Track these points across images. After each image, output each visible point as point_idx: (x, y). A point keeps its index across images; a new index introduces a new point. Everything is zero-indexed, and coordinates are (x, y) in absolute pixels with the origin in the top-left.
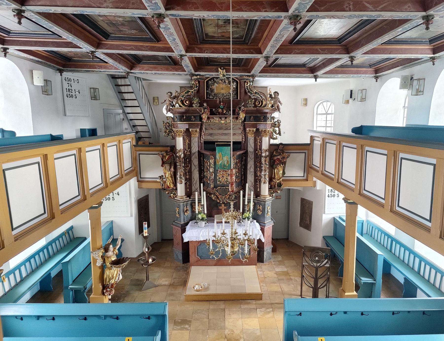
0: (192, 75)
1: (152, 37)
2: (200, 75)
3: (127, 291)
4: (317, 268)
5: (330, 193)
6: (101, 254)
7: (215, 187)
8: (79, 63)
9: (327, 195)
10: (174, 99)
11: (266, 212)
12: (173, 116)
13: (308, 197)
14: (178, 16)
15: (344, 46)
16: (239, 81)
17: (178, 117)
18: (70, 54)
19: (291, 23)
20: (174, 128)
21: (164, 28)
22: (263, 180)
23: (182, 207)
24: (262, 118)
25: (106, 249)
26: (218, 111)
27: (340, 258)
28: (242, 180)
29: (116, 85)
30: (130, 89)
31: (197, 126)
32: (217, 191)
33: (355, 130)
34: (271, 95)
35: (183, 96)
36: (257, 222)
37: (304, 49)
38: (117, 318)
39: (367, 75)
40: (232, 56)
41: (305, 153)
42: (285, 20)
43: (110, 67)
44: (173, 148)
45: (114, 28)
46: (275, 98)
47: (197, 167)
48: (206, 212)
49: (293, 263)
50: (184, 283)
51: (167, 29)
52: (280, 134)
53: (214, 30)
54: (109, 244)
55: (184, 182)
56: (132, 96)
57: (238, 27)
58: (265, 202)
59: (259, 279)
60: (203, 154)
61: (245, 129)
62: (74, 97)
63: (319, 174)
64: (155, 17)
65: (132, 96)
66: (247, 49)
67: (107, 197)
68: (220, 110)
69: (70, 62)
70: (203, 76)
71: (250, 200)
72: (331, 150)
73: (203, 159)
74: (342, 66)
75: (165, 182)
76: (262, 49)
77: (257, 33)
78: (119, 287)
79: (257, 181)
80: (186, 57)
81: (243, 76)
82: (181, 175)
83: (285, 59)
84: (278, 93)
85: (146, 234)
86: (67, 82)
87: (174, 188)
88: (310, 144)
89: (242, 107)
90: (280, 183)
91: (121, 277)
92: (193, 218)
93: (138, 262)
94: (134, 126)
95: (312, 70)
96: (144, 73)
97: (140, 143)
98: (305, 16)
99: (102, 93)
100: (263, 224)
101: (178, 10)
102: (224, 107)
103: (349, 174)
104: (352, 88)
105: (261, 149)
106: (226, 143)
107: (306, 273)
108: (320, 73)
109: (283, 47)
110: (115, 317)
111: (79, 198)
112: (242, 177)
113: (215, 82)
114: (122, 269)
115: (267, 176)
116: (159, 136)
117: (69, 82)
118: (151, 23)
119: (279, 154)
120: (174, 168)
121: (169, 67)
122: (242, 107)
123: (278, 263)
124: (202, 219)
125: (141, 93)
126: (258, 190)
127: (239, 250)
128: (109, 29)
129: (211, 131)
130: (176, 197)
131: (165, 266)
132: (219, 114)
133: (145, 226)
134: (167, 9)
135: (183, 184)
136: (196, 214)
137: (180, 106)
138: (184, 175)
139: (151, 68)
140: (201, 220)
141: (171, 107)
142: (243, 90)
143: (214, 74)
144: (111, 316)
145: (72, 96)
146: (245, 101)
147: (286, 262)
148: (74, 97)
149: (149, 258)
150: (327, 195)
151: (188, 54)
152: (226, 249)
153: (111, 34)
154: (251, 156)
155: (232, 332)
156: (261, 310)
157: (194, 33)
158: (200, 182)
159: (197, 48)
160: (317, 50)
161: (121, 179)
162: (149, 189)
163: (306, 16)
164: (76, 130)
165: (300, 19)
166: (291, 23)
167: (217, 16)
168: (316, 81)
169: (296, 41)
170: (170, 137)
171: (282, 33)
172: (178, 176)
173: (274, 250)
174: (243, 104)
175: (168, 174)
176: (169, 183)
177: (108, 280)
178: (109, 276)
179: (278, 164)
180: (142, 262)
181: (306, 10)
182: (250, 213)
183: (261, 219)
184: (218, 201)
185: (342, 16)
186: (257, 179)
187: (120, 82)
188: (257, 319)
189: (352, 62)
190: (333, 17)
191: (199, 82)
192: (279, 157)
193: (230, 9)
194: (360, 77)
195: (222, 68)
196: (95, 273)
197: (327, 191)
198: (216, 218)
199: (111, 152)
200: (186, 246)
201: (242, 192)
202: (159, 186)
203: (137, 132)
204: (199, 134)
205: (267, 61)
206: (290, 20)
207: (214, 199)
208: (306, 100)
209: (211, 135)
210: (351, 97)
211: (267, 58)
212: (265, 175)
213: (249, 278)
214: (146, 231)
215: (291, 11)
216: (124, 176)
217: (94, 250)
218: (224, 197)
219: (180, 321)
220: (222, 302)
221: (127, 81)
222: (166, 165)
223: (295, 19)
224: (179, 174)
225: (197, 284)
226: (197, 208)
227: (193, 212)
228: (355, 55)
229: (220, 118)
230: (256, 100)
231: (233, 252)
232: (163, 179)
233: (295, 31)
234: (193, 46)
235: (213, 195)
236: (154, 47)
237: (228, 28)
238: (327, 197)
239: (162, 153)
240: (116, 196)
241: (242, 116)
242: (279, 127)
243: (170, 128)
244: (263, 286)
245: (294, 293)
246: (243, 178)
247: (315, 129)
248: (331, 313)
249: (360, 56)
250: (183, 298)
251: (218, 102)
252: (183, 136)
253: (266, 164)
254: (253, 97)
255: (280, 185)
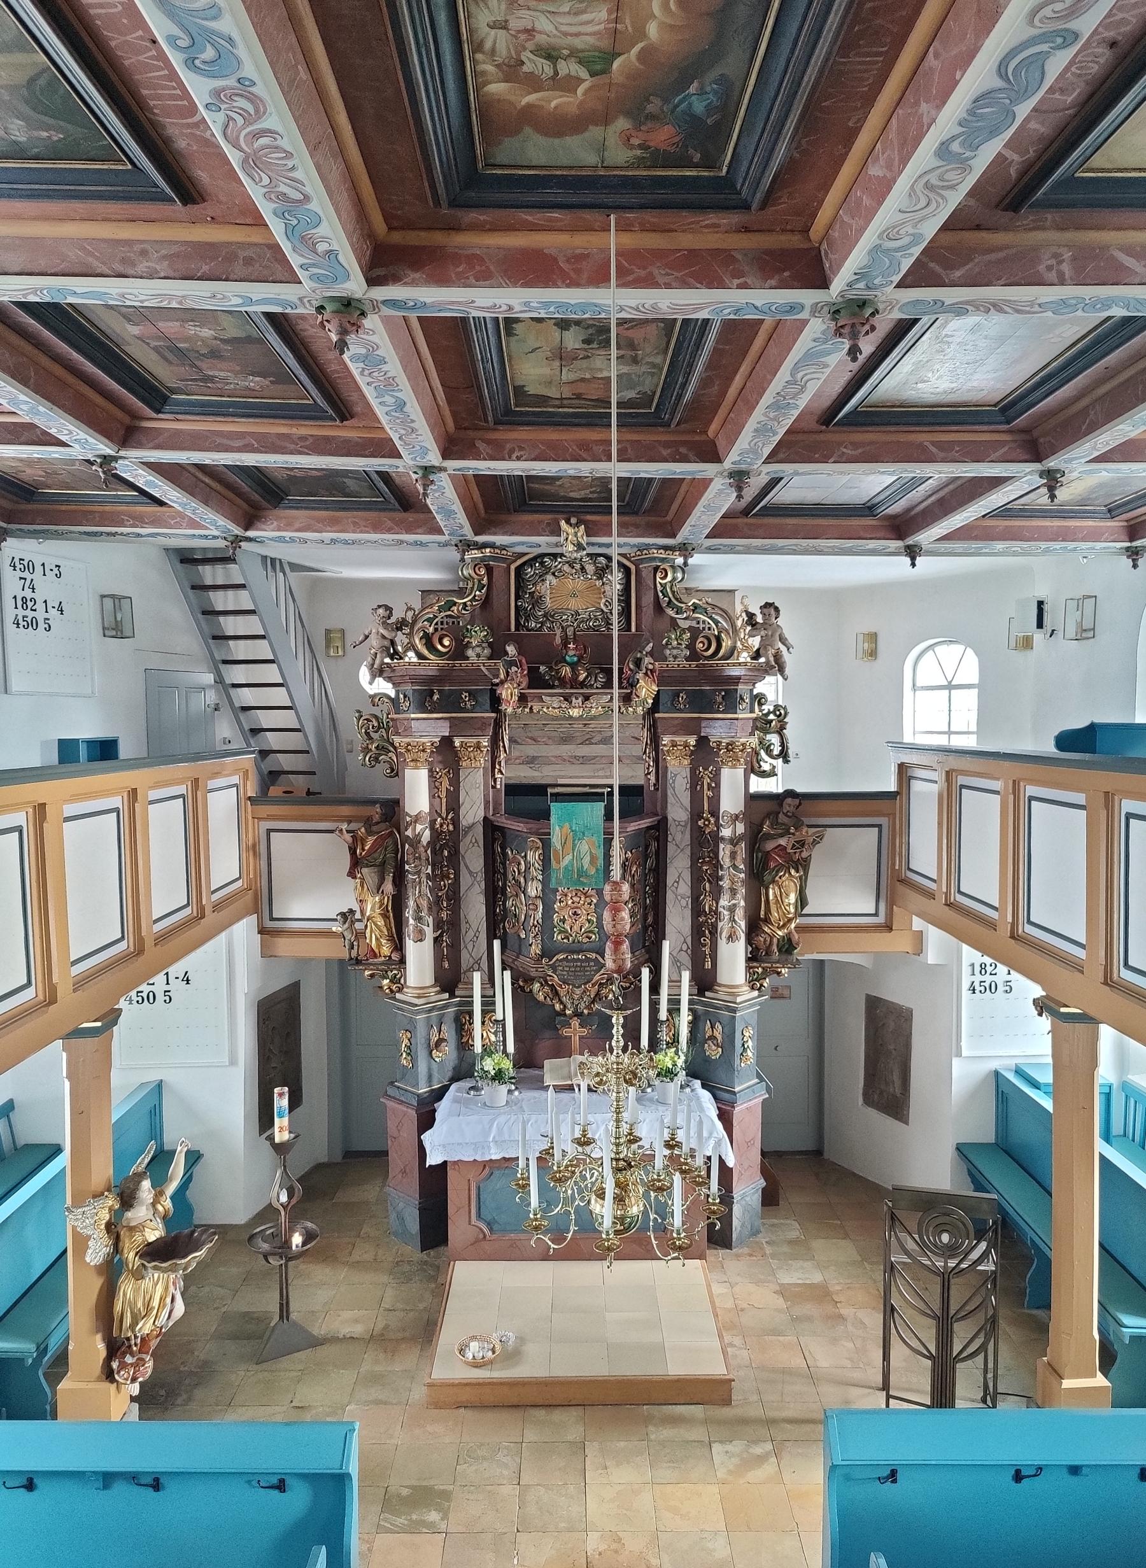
0: (468, 545)
1: (320, 401)
2: (492, 546)
3: (206, 1363)
4: (946, 1279)
5: (978, 978)
6: (105, 1216)
7: (547, 953)
8: (63, 508)
9: (965, 985)
10: (399, 629)
11: (738, 1049)
12: (392, 694)
13: (895, 992)
14: (414, 308)
15: (1022, 431)
16: (633, 568)
17: (410, 694)
18: (29, 471)
19: (838, 332)
20: (397, 734)
21: (363, 359)
22: (724, 926)
23: (421, 1031)
24: (719, 699)
25: (127, 1199)
26: (557, 671)
27: (1031, 1233)
28: (645, 928)
29: (193, 587)
30: (243, 600)
31: (481, 725)
32: (554, 968)
33: (1066, 741)
34: (751, 616)
35: (430, 620)
36: (704, 1086)
37: (872, 443)
38: (156, 1485)
39: (1099, 545)
40: (616, 470)
41: (879, 826)
42: (813, 321)
43: (174, 518)
44: (392, 809)
45: (184, 371)
46: (766, 625)
47: (481, 877)
48: (511, 1049)
49: (842, 1250)
50: (426, 1331)
51: (371, 360)
52: (784, 755)
53: (546, 371)
54: (139, 1177)
55: (429, 933)
56: (251, 625)
57: (635, 361)
58: (734, 1011)
59: (716, 1315)
60: (502, 830)
61: (655, 741)
62: (42, 625)
63: (937, 907)
64: (329, 308)
65: (251, 625)
66: (667, 445)
67: (145, 988)
68: (566, 671)
69: (28, 501)
70: (503, 548)
71: (678, 1002)
72: (983, 813)
73: (503, 849)
74: (1005, 512)
75: (360, 935)
76: (721, 443)
77: (705, 383)
78: (169, 1345)
79: (704, 930)
80: (443, 475)
81: (648, 547)
82: (418, 909)
83: (808, 483)
84: (777, 609)
85: (281, 1135)
86: (19, 574)
87: (395, 957)
88: (897, 793)
89: (648, 660)
90: (790, 940)
91: (180, 1308)
92: (464, 1071)
93: (258, 1237)
94: (255, 731)
95: (900, 528)
96: (292, 540)
97: (275, 791)
98: (891, 305)
99: (142, 613)
100: (726, 1096)
101: (414, 283)
102: (580, 658)
103: (1060, 906)
104: (1041, 594)
105: (715, 812)
106: (587, 790)
107: (903, 1296)
108: (925, 537)
109: (800, 437)
110: (149, 1480)
111: (29, 994)
112: (645, 918)
113: (547, 570)
114: (186, 1278)
115: (740, 914)
116: (343, 768)
117: (26, 574)
118: (310, 331)
119: (784, 830)
120: (394, 881)
121: (384, 516)
122: (648, 660)
123: (785, 1249)
124: (499, 1076)
125: (283, 614)
126: (708, 965)
127: (645, 1213)
128: (164, 372)
129: (531, 750)
130: (400, 990)
131: (356, 1256)
132: (563, 683)
133: (281, 1102)
134: (372, 282)
135: (428, 943)
136: (474, 1056)
137: (420, 656)
138: (430, 909)
139: (319, 520)
140: (493, 1079)
141: (387, 660)
142: (648, 599)
143: (542, 542)
144: (133, 1478)
145: (33, 624)
146: (656, 636)
147: (818, 1244)
148: (42, 625)
149: (291, 1231)
150: (965, 985)
151: (453, 464)
152: (596, 1207)
153: (173, 391)
154: (678, 837)
155: (614, 1546)
156: (729, 1447)
157: (473, 384)
158: (491, 936)
159: (483, 440)
160: (921, 447)
161: (198, 922)
162: (304, 962)
163: (894, 302)
164: (45, 744)
165: (873, 315)
166: (838, 332)
167: (560, 306)
168: (913, 565)
169: (845, 417)
170: (382, 768)
171: (800, 375)
172: (409, 913)
173: (770, 1198)
174: (649, 648)
175: (372, 905)
176: (376, 938)
177: (128, 1320)
178: (132, 1305)
179: (780, 867)
180: (265, 1247)
181: (897, 279)
182: (677, 1053)
183: (721, 1074)
184: (558, 1007)
185: (1032, 304)
186: (701, 925)
187: (210, 574)
188: (715, 1489)
189: (1051, 489)
190: (997, 307)
191: (490, 570)
192: (782, 842)
193: (607, 279)
194: (1075, 549)
195: (573, 520)
196: (80, 1292)
197: (966, 970)
198: (551, 1070)
199: (164, 822)
200: (434, 1182)
201: (645, 973)
202: (339, 951)
203: (264, 754)
204: (488, 758)
205: (739, 489)
206: (834, 319)
207: (541, 997)
208: (873, 637)
209: (531, 761)
210: (1040, 625)
211: (739, 477)
212: (732, 909)
213: (675, 1311)
214: (285, 1121)
215: (838, 285)
216: (208, 910)
217: (78, 1202)
218: (578, 991)
219: (405, 1492)
220: (575, 1412)
221: (234, 573)
222: (365, 870)
223: (854, 315)
224: (411, 903)
225: (474, 1338)
226: (478, 1034)
227: (464, 1046)
228: (1062, 466)
229: (567, 698)
230: (695, 632)
231: (622, 1219)
232: (353, 923)
233: (854, 359)
234: (471, 434)
235: (537, 986)
236: (327, 439)
237: (598, 362)
238: (965, 993)
239: (353, 826)
240: (177, 986)
241: (646, 690)
242: (780, 731)
243: (381, 732)
244: (731, 1345)
245: (857, 1375)
246: (650, 920)
247: (908, 738)
248: (1018, 1472)
249: (1083, 471)
250: (419, 1393)
251: (558, 640)
252: (430, 763)
253: (735, 867)
254: (684, 624)
255: (788, 946)
